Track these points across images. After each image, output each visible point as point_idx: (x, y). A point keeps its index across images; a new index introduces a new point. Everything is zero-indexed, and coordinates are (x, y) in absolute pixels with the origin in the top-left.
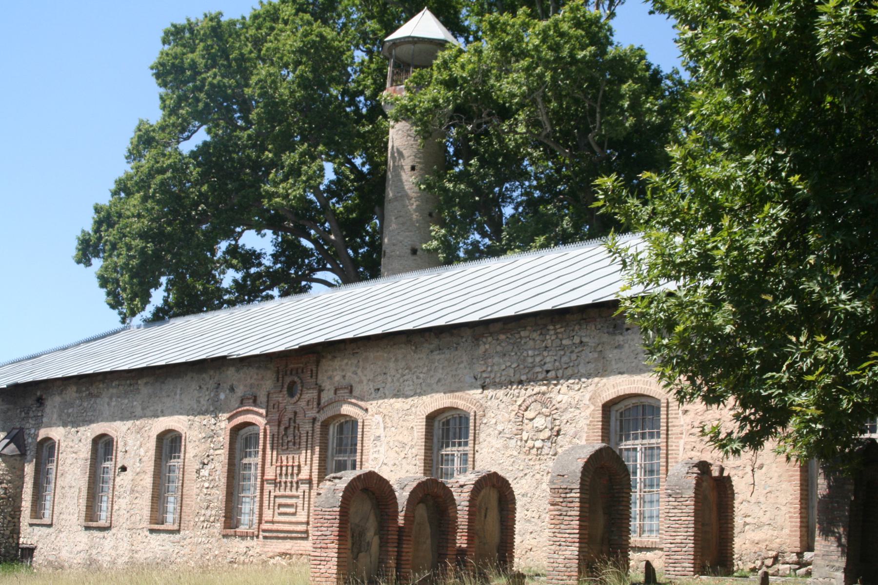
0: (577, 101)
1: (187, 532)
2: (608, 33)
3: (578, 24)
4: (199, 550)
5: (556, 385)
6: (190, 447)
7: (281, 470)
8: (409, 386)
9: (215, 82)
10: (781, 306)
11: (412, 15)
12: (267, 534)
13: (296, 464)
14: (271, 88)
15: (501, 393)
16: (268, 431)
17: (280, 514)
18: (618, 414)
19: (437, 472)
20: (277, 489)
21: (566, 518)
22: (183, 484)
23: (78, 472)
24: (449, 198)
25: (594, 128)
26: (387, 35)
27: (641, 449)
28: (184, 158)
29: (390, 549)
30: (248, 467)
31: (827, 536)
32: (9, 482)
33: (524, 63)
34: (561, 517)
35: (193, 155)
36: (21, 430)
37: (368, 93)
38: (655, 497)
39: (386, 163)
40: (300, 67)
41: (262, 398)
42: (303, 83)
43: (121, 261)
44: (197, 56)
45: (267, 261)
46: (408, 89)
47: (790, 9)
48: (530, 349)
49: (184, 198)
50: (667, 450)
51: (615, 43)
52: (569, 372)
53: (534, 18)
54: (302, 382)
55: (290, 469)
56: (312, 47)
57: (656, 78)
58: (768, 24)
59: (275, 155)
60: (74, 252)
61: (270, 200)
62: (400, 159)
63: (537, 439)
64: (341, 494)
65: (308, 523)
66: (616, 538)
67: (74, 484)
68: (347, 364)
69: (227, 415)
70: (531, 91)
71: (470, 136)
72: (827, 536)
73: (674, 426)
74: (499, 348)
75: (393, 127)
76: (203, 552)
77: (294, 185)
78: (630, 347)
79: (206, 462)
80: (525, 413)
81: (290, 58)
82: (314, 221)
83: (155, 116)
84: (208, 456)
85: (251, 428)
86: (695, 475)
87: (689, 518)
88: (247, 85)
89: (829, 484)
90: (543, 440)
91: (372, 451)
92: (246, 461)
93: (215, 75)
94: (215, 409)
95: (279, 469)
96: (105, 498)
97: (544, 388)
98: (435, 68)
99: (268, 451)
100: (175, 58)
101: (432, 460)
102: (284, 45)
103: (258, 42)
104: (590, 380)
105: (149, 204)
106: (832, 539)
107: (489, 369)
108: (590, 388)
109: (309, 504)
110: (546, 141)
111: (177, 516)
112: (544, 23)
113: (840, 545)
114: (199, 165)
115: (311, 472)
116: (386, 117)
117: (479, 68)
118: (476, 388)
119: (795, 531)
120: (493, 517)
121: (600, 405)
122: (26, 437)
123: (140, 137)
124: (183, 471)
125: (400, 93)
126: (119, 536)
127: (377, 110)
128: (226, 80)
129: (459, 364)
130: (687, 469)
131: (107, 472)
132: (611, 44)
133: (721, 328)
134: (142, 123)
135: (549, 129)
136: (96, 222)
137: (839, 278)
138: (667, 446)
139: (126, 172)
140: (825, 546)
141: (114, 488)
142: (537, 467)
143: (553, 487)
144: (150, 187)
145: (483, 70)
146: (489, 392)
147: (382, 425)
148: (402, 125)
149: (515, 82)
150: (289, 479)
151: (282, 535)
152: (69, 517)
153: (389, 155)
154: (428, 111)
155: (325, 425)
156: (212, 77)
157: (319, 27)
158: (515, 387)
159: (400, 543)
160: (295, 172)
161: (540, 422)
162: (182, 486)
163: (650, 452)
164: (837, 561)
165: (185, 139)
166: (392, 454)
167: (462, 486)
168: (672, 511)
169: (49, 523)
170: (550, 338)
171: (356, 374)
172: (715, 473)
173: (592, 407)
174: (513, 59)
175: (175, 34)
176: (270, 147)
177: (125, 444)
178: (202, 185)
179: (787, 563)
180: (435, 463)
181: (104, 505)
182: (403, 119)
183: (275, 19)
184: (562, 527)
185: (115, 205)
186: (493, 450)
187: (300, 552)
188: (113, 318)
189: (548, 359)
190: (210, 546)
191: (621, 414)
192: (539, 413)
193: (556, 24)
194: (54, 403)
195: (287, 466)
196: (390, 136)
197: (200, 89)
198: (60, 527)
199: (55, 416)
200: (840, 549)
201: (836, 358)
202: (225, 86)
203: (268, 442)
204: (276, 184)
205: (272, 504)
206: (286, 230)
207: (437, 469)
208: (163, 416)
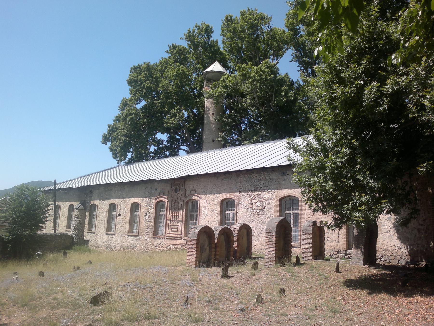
0: (267, 92)
1: (141, 236)
2: (277, 70)
3: (267, 67)
4: (145, 242)
5: (264, 192)
6: (142, 208)
7: (173, 217)
8: (215, 190)
9: (148, 85)
10: (349, 183)
11: (212, 63)
12: (168, 238)
13: (178, 215)
14: (166, 87)
15: (245, 194)
16: (168, 204)
17: (172, 231)
18: (284, 202)
19: (224, 219)
20: (171, 223)
21: (271, 242)
22: (140, 220)
23: (104, 215)
24: (225, 124)
25: (272, 101)
26: (205, 70)
27: (292, 214)
28: (138, 110)
29: (213, 251)
30: (161, 215)
31: (357, 248)
32: (80, 218)
33: (250, 81)
34: (269, 242)
35: (141, 109)
36: (85, 201)
37: (198, 89)
38: (297, 230)
39: (204, 111)
40: (176, 81)
41: (166, 193)
42: (178, 86)
43: (118, 144)
44: (141, 77)
45: (165, 143)
46: (211, 88)
47: (354, 87)
48: (255, 180)
49: (138, 123)
50: (301, 215)
51: (279, 73)
52: (268, 188)
53: (253, 66)
54: (179, 188)
55: (175, 216)
56: (180, 74)
57: (292, 83)
58: (347, 92)
59: (168, 109)
60: (101, 140)
61: (167, 124)
62: (209, 111)
63: (257, 209)
64: (197, 234)
65: (181, 234)
66: (287, 248)
67: (103, 219)
68: (194, 183)
69: (154, 198)
70: (252, 90)
71: (232, 103)
72: (357, 248)
73: (303, 207)
74: (245, 179)
75: (206, 101)
76: (146, 243)
77: (174, 120)
78: (288, 180)
79: (147, 213)
80: (254, 201)
81: (172, 78)
82: (180, 130)
83: (128, 96)
84: (148, 211)
85: (162, 202)
86: (312, 226)
87: (310, 240)
88: (158, 86)
89: (358, 231)
90: (259, 210)
91: (203, 211)
92: (161, 213)
93: (148, 84)
94: (150, 196)
95: (172, 216)
96: (113, 224)
97: (260, 193)
98: (220, 81)
99: (168, 210)
100: (135, 77)
101: (223, 215)
102: (171, 73)
103: (162, 72)
104: (275, 191)
105: (126, 125)
106: (359, 249)
107: (242, 186)
108: (275, 193)
109: (182, 228)
110: (256, 105)
111: (137, 231)
112: (257, 67)
113: (362, 252)
114: (143, 113)
115: (182, 218)
116: (204, 97)
117: (235, 82)
118: (238, 192)
119: (344, 243)
120: (245, 238)
121: (279, 199)
122: (86, 203)
123: (123, 103)
124: (140, 216)
125: (209, 90)
126: (118, 237)
127: (200, 94)
128: (152, 85)
129: (232, 184)
130: (309, 224)
131: (114, 216)
132: (278, 74)
133: (328, 190)
134: (124, 98)
135: (258, 102)
136: (108, 130)
137: (368, 174)
138: (301, 213)
139: (119, 114)
140: (356, 252)
141: (116, 221)
142: (258, 218)
143: (267, 232)
144: (127, 120)
145: (237, 83)
146: (242, 194)
147: (206, 203)
148: (210, 100)
149: (247, 87)
150: (175, 220)
151: (173, 238)
152: (101, 230)
153: (205, 109)
154: (218, 96)
155: (187, 202)
156: (147, 84)
157: (182, 67)
158: (250, 192)
159: (216, 248)
160: (175, 115)
161: (258, 204)
162: (139, 221)
163: (296, 215)
164: (360, 257)
165: (138, 104)
166: (209, 213)
167: (235, 229)
168: (304, 238)
169: (94, 232)
170: (262, 176)
171: (197, 186)
172: (319, 225)
173: (276, 200)
174: (246, 79)
175: (134, 69)
176: (166, 107)
177: (120, 207)
178: (144, 119)
179: (342, 254)
180: (223, 216)
181: (113, 227)
182: (210, 98)
183: (167, 64)
184: (270, 245)
185: (115, 125)
186: (243, 212)
187: (179, 244)
188: (114, 162)
189: (261, 183)
190: (149, 241)
191: (285, 202)
192: (258, 201)
193: (261, 68)
194: (96, 192)
195: (175, 216)
196: (205, 103)
197: (143, 88)
198: (98, 234)
199: (96, 197)
200: (362, 253)
201: (368, 201)
202: (151, 87)
203: (168, 207)
204: (168, 119)
205: (169, 228)
206: (172, 133)
207: (224, 218)
208: (133, 198)
